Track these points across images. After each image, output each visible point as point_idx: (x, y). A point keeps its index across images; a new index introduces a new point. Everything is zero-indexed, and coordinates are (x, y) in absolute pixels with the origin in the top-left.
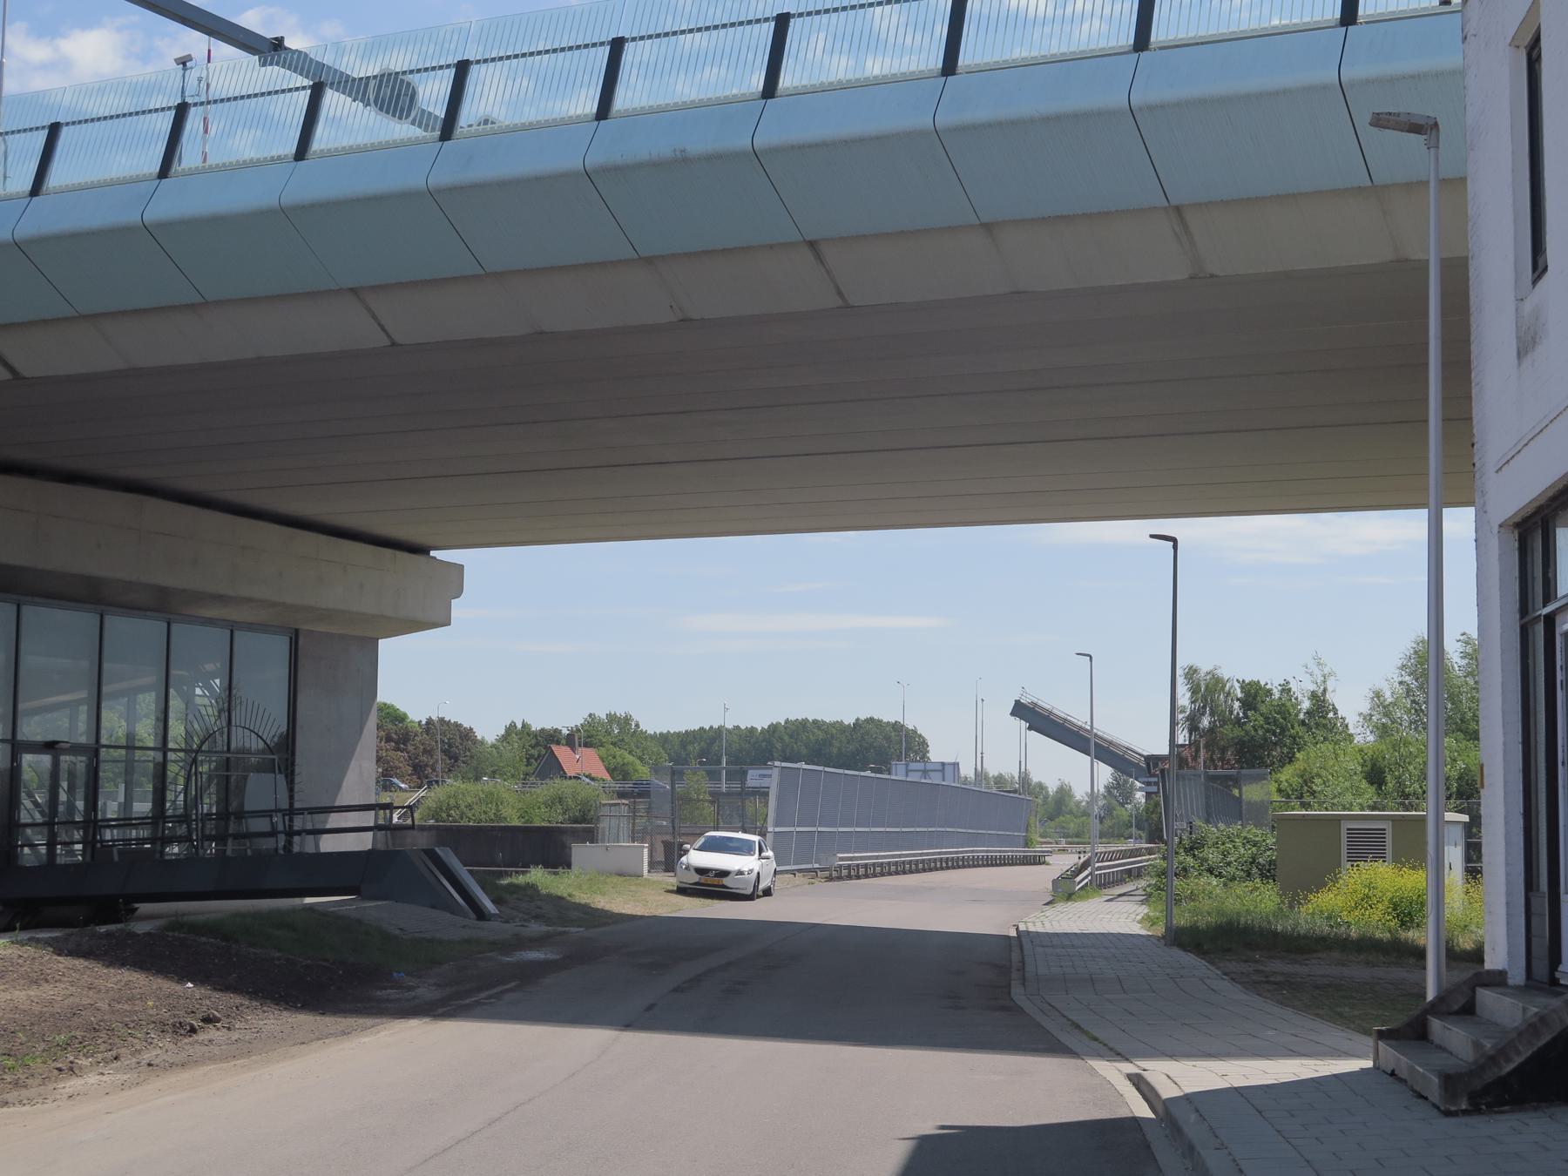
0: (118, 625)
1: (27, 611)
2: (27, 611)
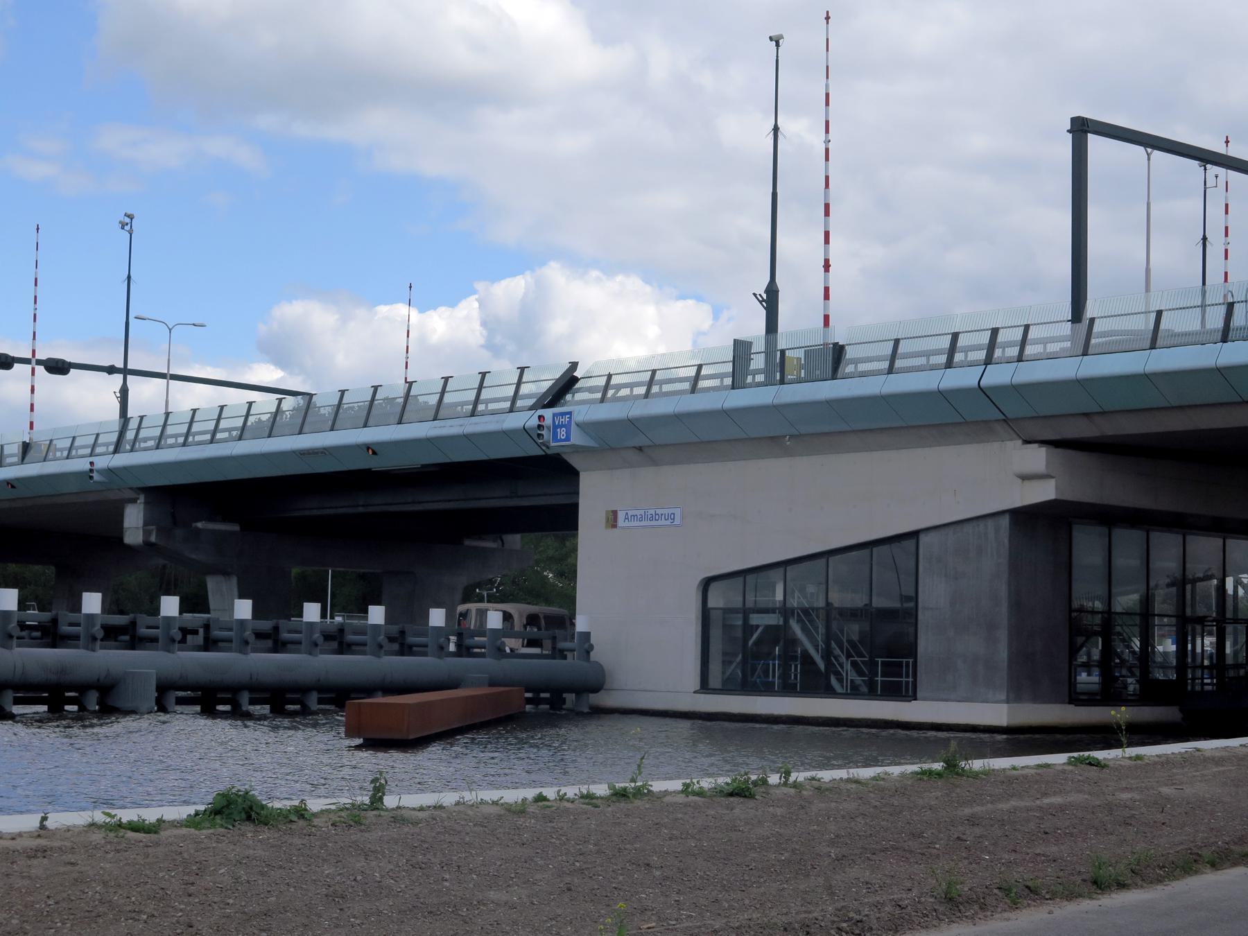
0: (1158, 538)
1: (1189, 538)
2: (1189, 538)
